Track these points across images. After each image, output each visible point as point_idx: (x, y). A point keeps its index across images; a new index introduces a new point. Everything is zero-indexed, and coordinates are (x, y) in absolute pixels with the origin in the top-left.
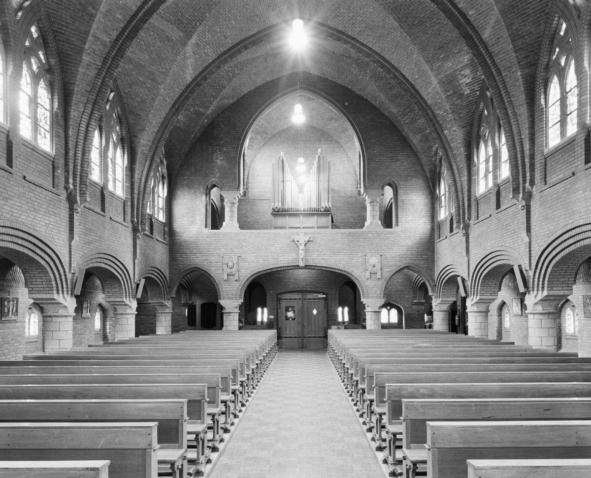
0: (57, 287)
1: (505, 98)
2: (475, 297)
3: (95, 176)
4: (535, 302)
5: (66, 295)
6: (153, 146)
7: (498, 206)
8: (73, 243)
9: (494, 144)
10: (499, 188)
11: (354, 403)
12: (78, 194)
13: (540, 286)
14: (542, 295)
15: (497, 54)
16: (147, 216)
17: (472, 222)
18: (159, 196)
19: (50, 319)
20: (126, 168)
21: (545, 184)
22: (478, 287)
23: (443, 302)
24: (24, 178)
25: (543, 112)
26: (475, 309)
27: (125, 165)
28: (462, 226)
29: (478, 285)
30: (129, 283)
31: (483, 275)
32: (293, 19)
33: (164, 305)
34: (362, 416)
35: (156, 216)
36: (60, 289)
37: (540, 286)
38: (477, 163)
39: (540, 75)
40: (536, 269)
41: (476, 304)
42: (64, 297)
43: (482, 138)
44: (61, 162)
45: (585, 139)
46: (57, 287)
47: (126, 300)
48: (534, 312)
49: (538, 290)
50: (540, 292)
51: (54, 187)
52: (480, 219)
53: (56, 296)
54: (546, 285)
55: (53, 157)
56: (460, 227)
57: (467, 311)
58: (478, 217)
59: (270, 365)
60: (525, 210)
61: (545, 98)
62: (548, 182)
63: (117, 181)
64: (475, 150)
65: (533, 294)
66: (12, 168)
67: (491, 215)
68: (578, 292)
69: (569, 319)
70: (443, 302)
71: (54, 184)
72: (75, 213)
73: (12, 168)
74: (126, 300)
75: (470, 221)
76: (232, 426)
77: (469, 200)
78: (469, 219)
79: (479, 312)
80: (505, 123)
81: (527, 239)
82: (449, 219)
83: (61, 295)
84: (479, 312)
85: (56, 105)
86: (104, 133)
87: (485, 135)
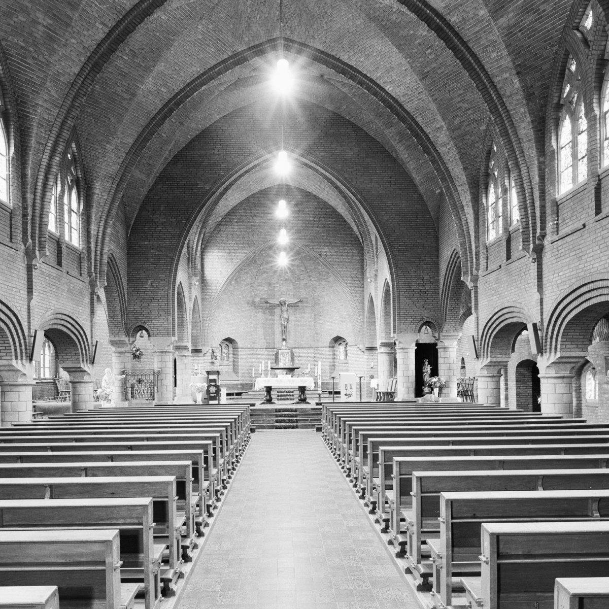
0: (16, 353)
1: (512, 137)
2: (553, 354)
3: (52, 227)
4: (548, 365)
5: (24, 361)
6: (114, 186)
7: (509, 257)
8: (33, 302)
9: (503, 186)
10: (510, 235)
11: (353, 484)
12: (37, 249)
13: (553, 347)
14: (554, 358)
15: (501, 89)
16: (48, 234)
17: (481, 273)
18: (71, 210)
19: (77, 384)
20: (13, 158)
21: (557, 234)
22: (557, 339)
23: (564, 360)
24: (68, 273)
25: (553, 155)
26: (552, 373)
27: (81, 211)
28: (531, 246)
29: (557, 336)
30: (21, 337)
31: (493, 335)
32: (278, 149)
33: (13, 370)
34: (362, 497)
35: (67, 238)
36: (19, 354)
37: (553, 347)
38: (485, 205)
39: (550, 112)
40: (481, 340)
41: (486, 367)
42: (22, 363)
43: (491, 177)
44: (19, 213)
45: (596, 188)
46: (16, 353)
47: (17, 363)
48: (547, 376)
49: (550, 352)
50: (553, 354)
51: (11, 241)
52: (562, 233)
53: (14, 362)
54: (559, 346)
55: (12, 208)
56: (529, 249)
57: (539, 376)
58: (487, 268)
59: (244, 453)
60: (536, 263)
61: (557, 139)
62: (489, 269)
63: (73, 229)
64: (484, 195)
65: (546, 356)
66: (61, 267)
67: (584, 226)
68: (595, 351)
69: (590, 384)
70: (564, 360)
71: (11, 238)
72: (33, 270)
73: (61, 267)
74: (17, 363)
75: (478, 272)
76: (215, 510)
77: (543, 207)
78: (478, 270)
79: (490, 377)
80: (514, 164)
81: (537, 296)
82: (505, 238)
83: (19, 361)
84: (490, 377)
85: (81, 208)
86: (82, 198)
87: (571, 102)
